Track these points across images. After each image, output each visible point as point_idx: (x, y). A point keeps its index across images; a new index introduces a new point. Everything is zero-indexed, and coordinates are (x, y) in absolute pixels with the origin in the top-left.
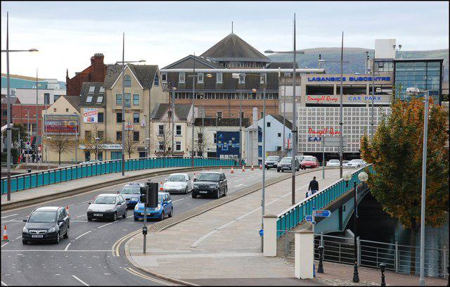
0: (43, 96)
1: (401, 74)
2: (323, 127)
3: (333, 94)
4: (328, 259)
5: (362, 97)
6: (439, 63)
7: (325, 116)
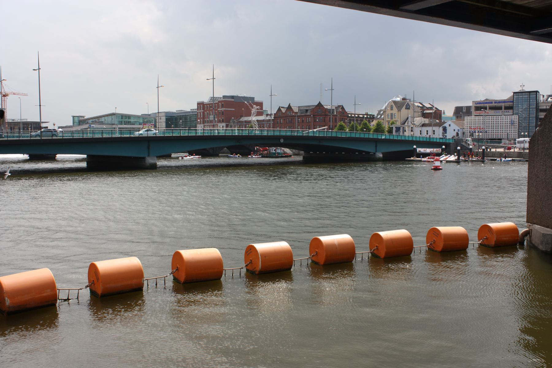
0: (334, 118)
3: (502, 110)
4: (39, 122)
6: (535, 93)
7: (477, 121)
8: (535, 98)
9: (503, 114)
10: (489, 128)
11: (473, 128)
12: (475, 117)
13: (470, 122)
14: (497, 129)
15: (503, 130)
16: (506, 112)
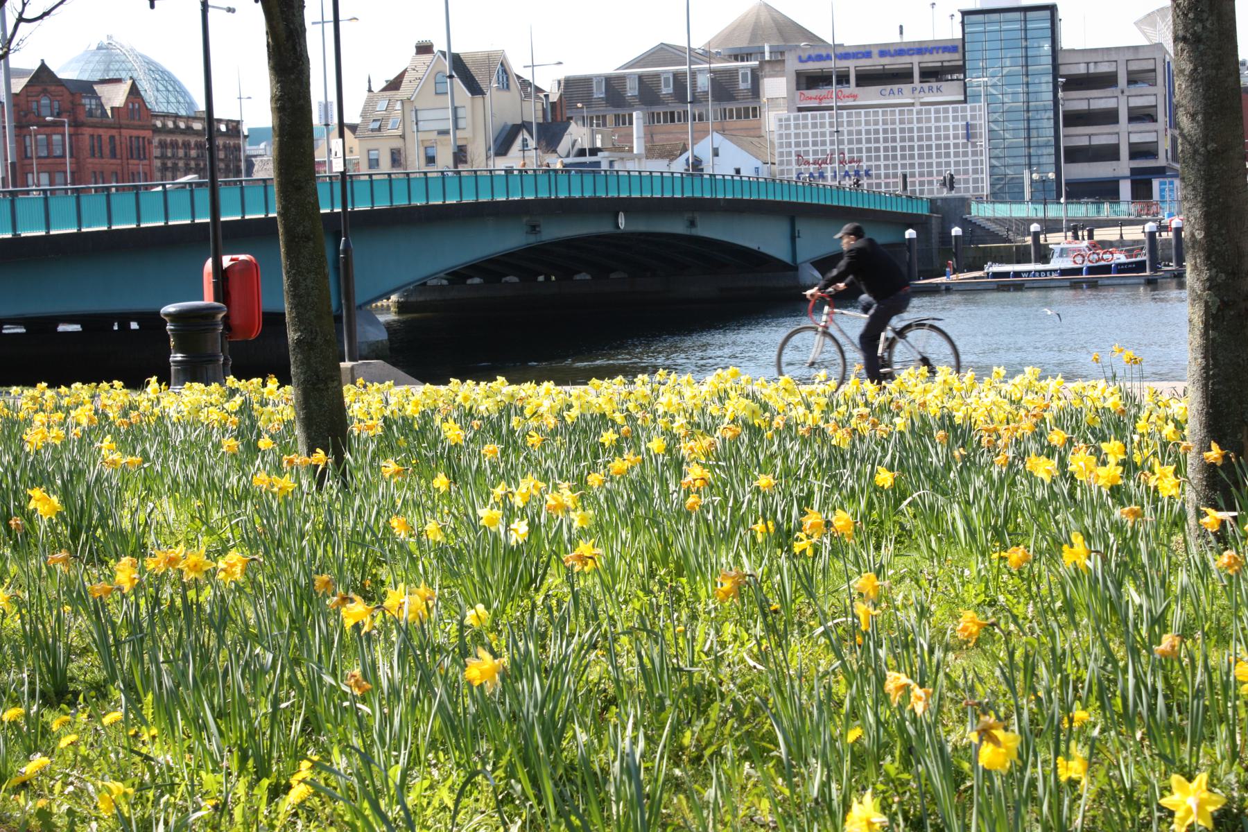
1: (977, 37)
2: (824, 152)
5: (906, 88)
6: (1047, 13)
8: (1049, 33)
9: (917, 101)
10: (878, 158)
11: (811, 158)
12: (801, 114)
14: (908, 162)
15: (930, 165)
16: (930, 89)
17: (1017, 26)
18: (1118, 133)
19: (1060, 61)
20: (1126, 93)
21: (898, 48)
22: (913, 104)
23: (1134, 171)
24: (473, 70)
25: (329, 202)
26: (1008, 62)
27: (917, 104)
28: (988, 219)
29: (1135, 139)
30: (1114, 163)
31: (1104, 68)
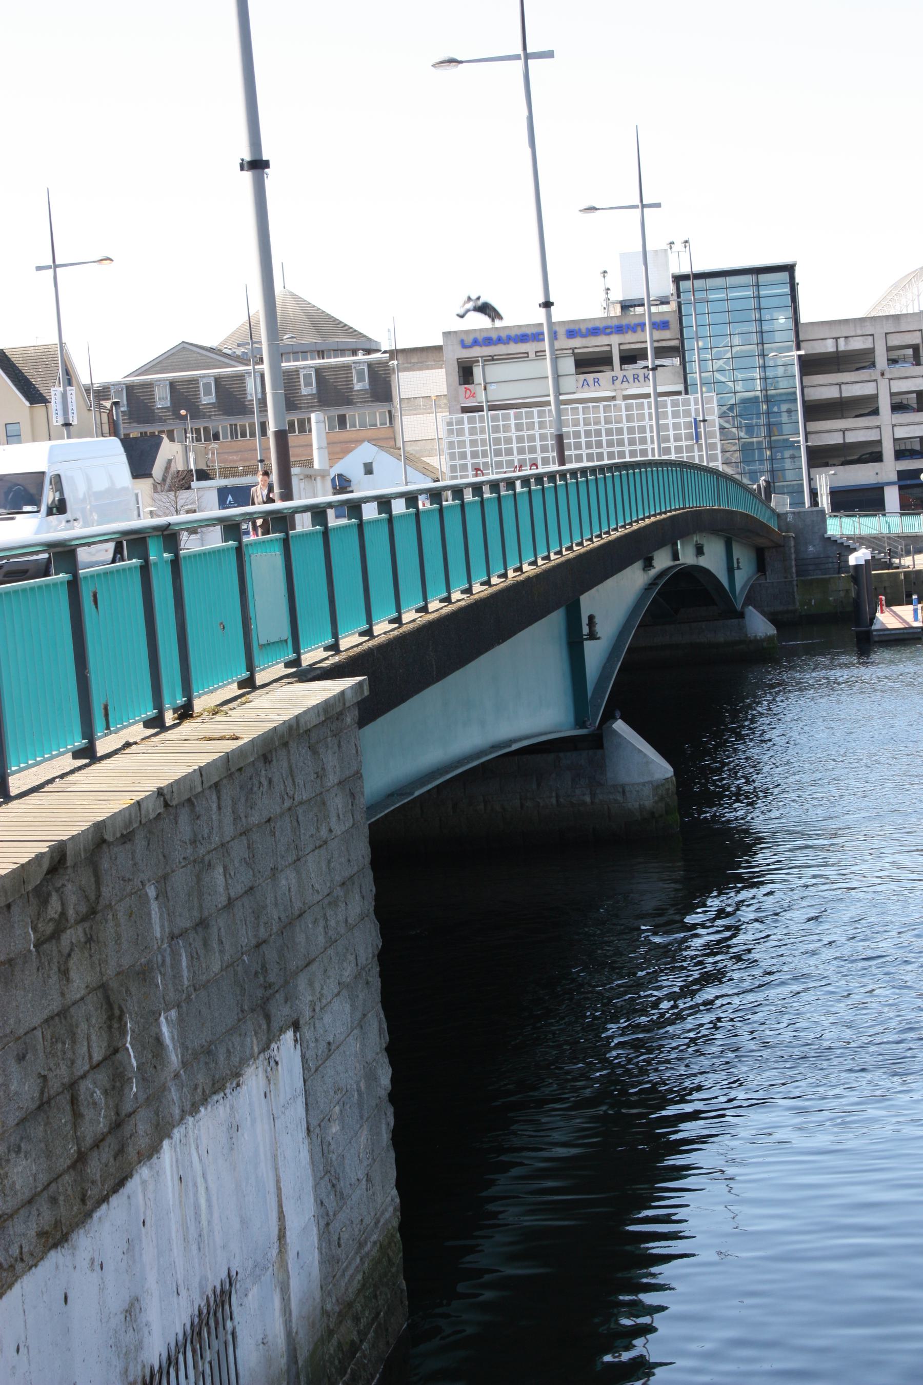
5: (605, 377)
6: (785, 276)
12: (465, 416)
13: (588, 434)
17: (749, 293)
18: (879, 427)
19: (801, 338)
20: (887, 376)
21: (590, 326)
22: (613, 398)
23: (902, 474)
24: (26, 370)
25: (546, 549)
26: (736, 340)
27: (619, 397)
28: (849, 538)
29: (901, 433)
30: (877, 465)
31: (857, 344)
